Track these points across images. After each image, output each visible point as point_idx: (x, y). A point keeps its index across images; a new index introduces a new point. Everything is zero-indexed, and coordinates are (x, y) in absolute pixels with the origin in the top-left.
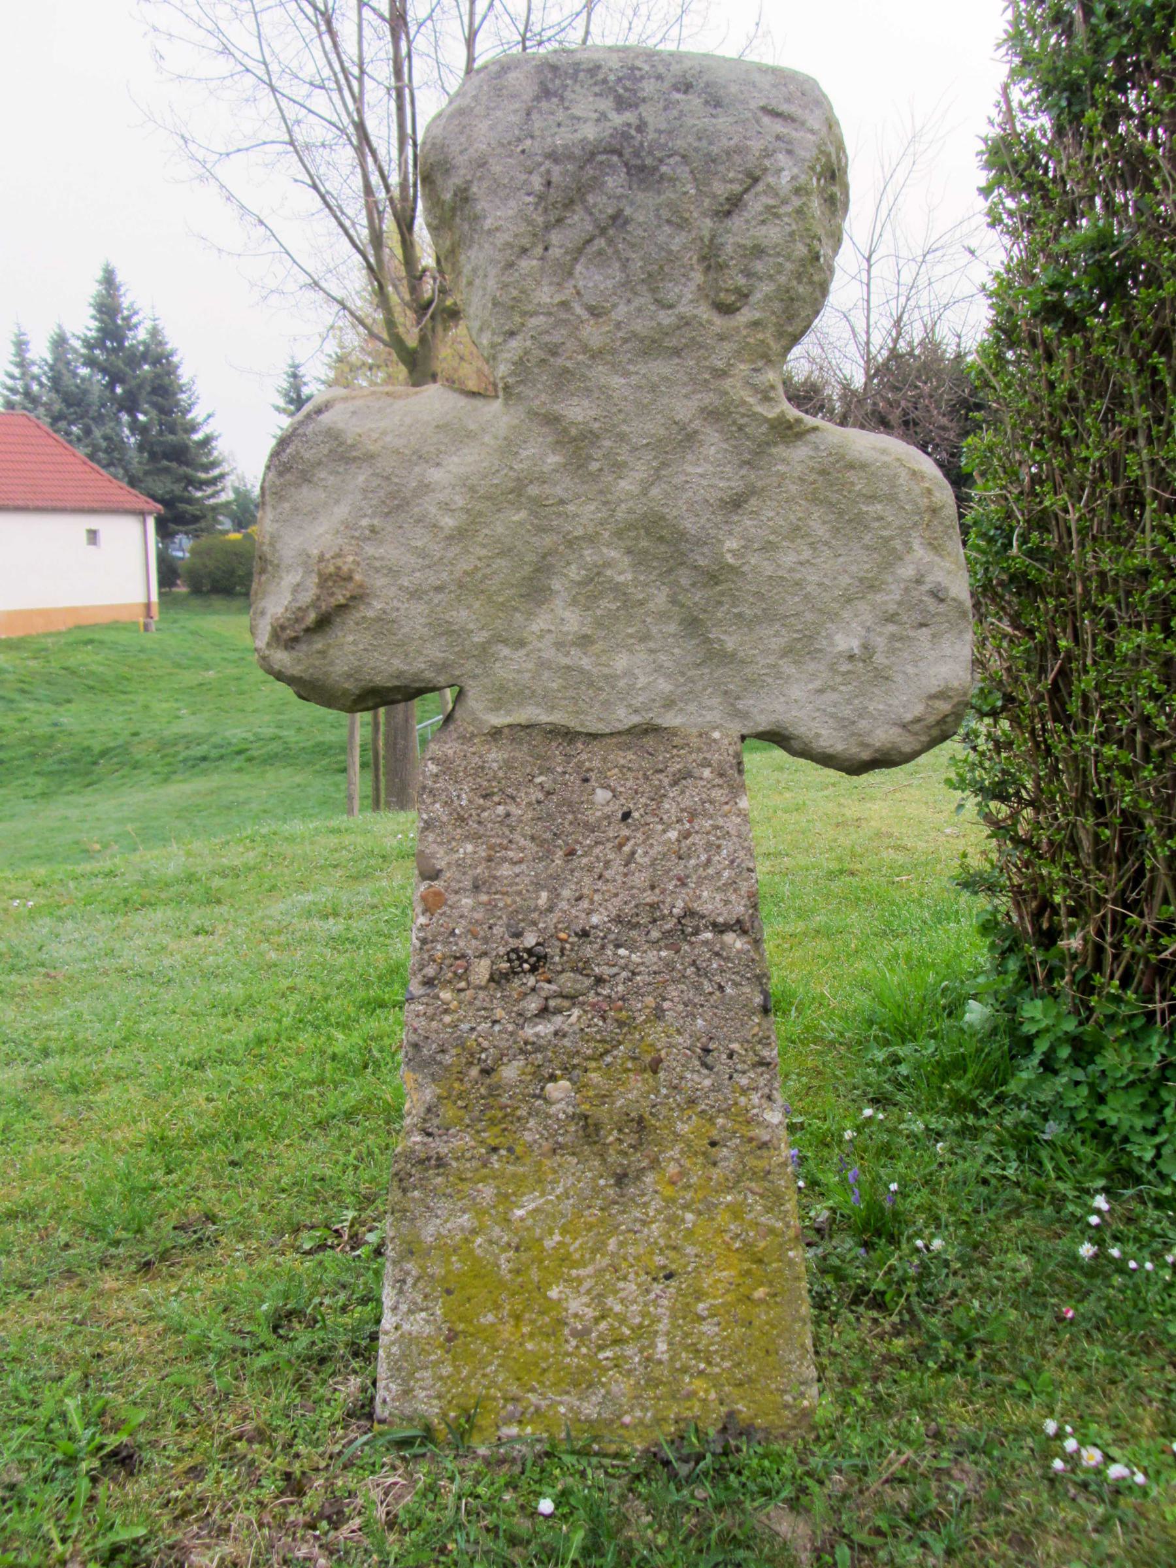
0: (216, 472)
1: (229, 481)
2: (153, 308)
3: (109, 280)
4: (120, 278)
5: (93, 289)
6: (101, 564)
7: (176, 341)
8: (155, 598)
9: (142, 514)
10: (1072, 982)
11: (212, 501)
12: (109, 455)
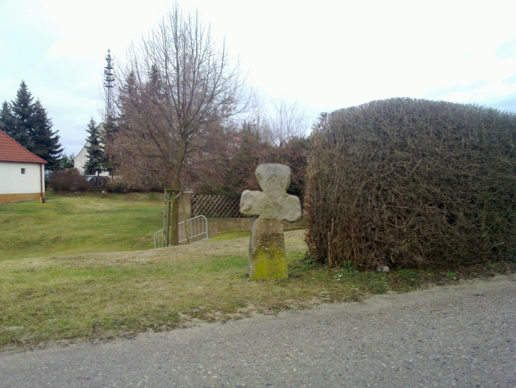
0: (60, 149)
1: (63, 153)
2: (38, 95)
3: (23, 85)
4: (26, 84)
5: (19, 88)
6: (27, 180)
7: (44, 105)
8: (44, 191)
9: (40, 164)
10: (341, 229)
11: (58, 159)
12: (22, 141)
